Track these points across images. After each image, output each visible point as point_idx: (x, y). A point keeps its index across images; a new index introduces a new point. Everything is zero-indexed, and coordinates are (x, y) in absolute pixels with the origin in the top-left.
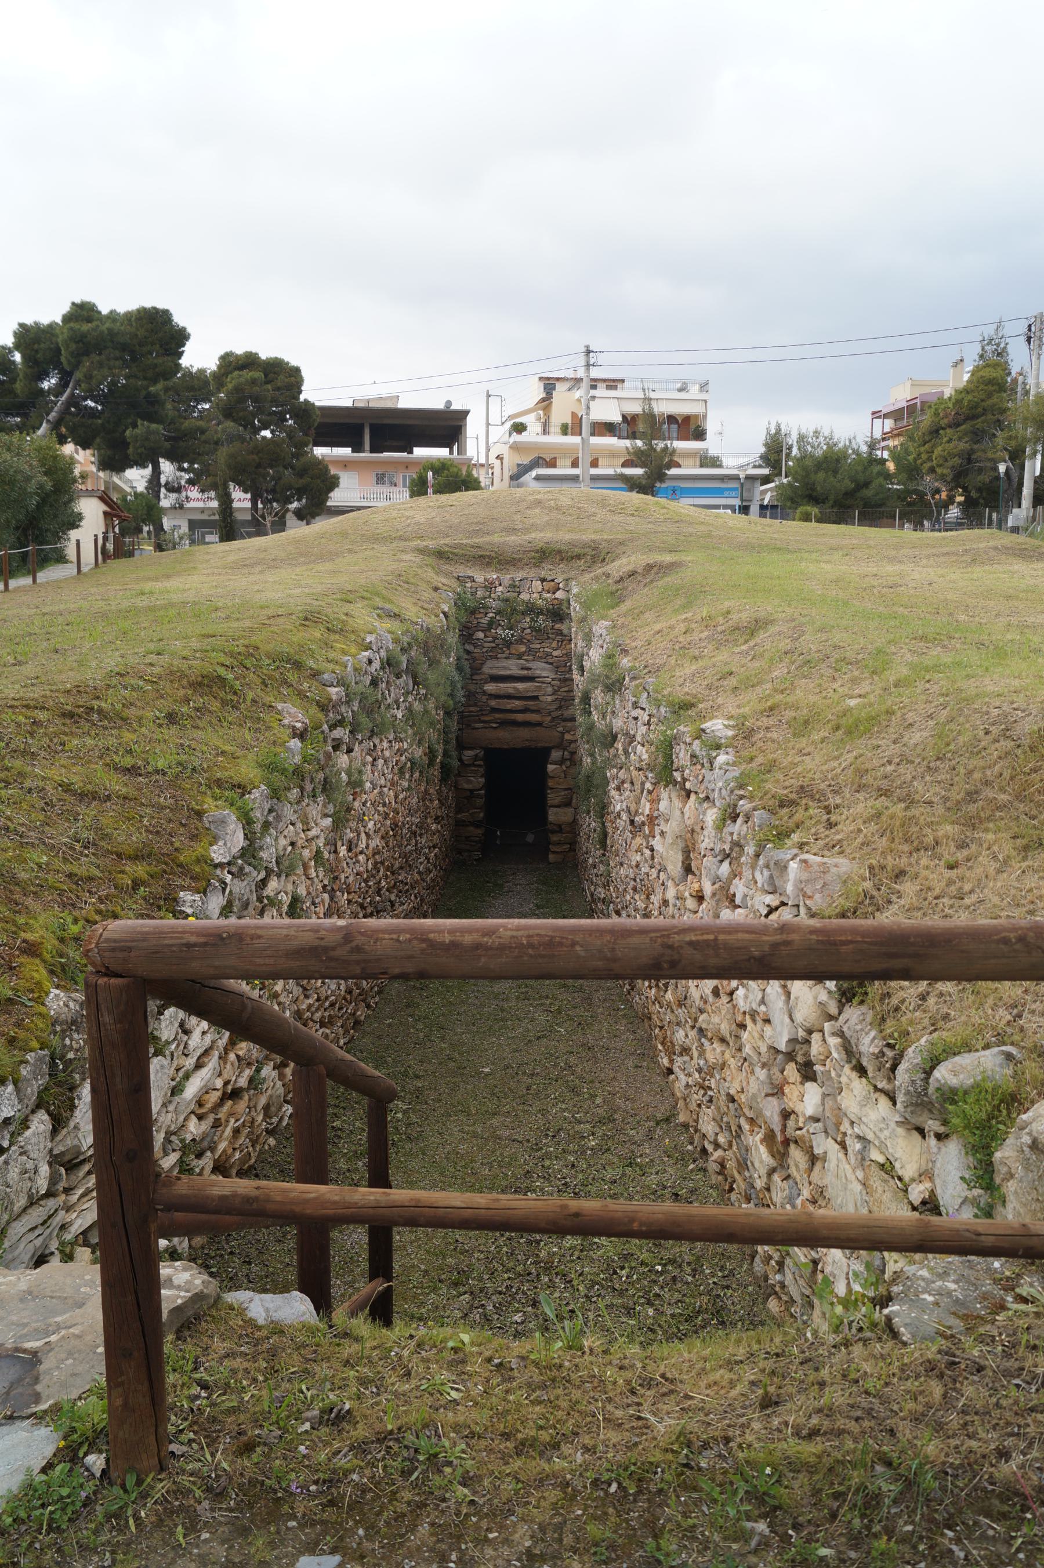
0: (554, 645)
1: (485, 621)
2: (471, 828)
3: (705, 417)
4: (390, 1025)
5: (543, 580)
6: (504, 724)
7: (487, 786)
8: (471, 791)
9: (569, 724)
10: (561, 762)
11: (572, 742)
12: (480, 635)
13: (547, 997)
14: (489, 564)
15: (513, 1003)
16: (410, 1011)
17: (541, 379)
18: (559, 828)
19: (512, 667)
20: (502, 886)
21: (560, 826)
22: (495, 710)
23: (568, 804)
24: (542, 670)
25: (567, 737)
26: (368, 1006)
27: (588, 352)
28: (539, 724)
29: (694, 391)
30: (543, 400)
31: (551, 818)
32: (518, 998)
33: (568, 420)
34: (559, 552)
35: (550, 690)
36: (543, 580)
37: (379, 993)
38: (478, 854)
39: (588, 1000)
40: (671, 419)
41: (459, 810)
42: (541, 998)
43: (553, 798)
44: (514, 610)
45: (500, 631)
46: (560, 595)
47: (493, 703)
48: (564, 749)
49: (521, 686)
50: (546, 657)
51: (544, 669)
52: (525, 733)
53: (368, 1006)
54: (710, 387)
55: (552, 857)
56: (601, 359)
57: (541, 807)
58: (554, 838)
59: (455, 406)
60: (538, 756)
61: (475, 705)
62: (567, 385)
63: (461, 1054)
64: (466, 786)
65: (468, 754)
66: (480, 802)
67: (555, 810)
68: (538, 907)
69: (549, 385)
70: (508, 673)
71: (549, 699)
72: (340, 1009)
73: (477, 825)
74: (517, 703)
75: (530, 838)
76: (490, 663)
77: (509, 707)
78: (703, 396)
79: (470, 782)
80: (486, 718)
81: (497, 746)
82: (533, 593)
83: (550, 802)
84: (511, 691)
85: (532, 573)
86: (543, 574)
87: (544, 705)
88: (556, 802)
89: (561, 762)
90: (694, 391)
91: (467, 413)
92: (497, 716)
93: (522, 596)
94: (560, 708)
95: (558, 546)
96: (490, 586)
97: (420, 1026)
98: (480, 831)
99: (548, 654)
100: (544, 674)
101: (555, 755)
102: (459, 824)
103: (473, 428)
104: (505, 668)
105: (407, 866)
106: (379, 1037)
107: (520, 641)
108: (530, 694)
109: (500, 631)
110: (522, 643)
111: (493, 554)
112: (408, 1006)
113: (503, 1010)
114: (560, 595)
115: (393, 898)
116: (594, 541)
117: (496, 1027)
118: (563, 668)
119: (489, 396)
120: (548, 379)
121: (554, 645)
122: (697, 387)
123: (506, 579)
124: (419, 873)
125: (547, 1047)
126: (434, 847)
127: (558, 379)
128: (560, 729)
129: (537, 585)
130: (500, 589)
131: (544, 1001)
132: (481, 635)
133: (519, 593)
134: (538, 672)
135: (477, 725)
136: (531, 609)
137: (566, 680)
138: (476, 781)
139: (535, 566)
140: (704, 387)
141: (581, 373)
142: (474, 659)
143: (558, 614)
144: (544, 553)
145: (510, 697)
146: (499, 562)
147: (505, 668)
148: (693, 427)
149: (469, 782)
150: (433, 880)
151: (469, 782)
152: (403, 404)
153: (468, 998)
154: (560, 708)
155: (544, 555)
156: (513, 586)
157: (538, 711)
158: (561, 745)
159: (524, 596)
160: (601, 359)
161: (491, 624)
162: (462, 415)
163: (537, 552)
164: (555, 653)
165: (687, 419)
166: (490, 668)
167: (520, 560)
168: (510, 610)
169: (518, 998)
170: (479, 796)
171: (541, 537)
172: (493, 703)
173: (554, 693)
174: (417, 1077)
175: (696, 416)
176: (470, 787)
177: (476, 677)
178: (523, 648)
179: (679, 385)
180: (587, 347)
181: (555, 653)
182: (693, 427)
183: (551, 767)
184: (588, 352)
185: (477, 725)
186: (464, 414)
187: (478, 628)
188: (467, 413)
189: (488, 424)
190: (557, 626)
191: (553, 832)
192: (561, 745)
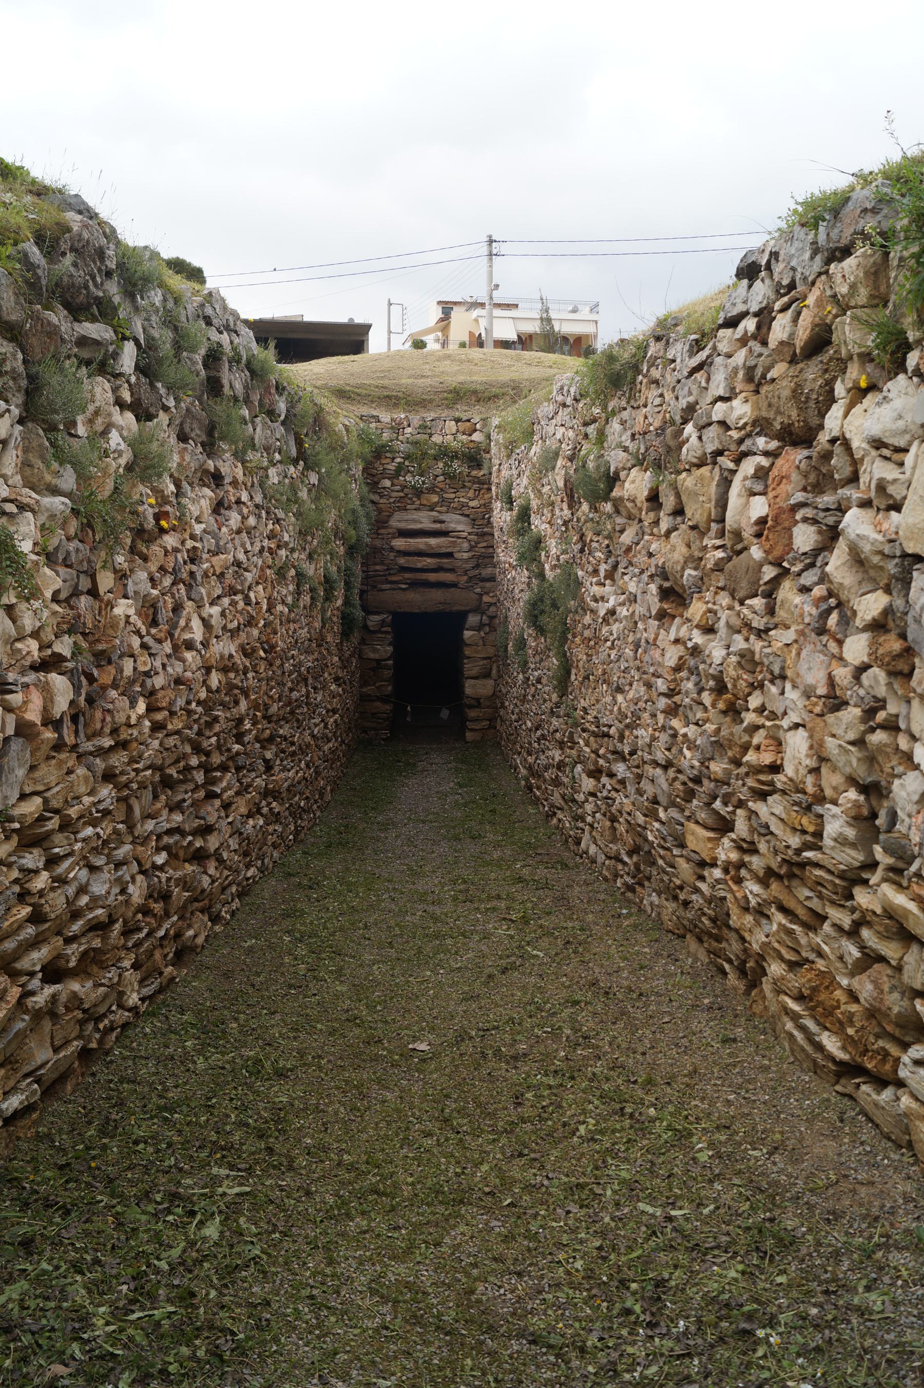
0: (471, 494)
1: (392, 467)
2: (378, 704)
3: (596, 336)
4: (250, 951)
5: (457, 420)
6: (415, 585)
7: (395, 656)
8: (378, 661)
9: (488, 585)
10: (479, 628)
11: (491, 604)
12: (387, 483)
13: (499, 897)
14: (396, 405)
15: (449, 907)
16: (287, 923)
17: (439, 303)
18: (477, 703)
19: (423, 520)
20: (414, 765)
21: (478, 700)
22: (404, 569)
23: (487, 675)
24: (457, 523)
25: (486, 599)
26: (216, 919)
27: (491, 241)
28: (454, 585)
29: (585, 313)
30: (442, 320)
31: (468, 691)
32: (455, 899)
33: (466, 339)
34: (475, 392)
35: (466, 545)
36: (457, 420)
37: (240, 895)
38: (385, 733)
39: (562, 900)
40: (565, 339)
41: (364, 683)
42: (490, 898)
43: (470, 668)
44: (424, 454)
45: (409, 478)
46: (476, 437)
47: (402, 561)
48: (483, 613)
49: (433, 541)
50: (461, 509)
51: (459, 522)
52: (437, 595)
53: (216, 919)
54: (600, 308)
55: (469, 736)
56: (503, 248)
57: (455, 678)
58: (472, 714)
59: (358, 320)
60: (454, 621)
61: (382, 563)
62: (463, 308)
63: (371, 1007)
64: (372, 656)
65: (374, 620)
66: (388, 673)
67: (472, 682)
68: (461, 786)
69: (447, 308)
70: (418, 526)
71: (466, 555)
72: (126, 933)
73: (384, 700)
74: (429, 560)
75: (445, 714)
76: (397, 516)
77: (419, 565)
78: (594, 317)
79: (377, 651)
80: (394, 578)
81: (407, 610)
82: (447, 434)
83: (467, 674)
84: (422, 547)
85: (446, 413)
86: (457, 414)
87: (459, 563)
88: (474, 672)
89: (479, 628)
90: (585, 313)
91: (368, 327)
92: (407, 575)
93: (434, 439)
94: (477, 566)
95: (473, 386)
96: (397, 428)
97: (301, 950)
98: (388, 707)
99: (464, 505)
100: (460, 528)
101: (473, 619)
102: (364, 699)
103: (376, 343)
104: (415, 521)
105: (291, 715)
106: (227, 975)
107: (432, 490)
108: (444, 550)
109: (409, 478)
110: (434, 492)
111: (400, 394)
112: (286, 915)
113: (436, 920)
114: (476, 437)
115: (269, 755)
116: (514, 381)
117: (428, 950)
118: (481, 522)
119: (390, 304)
120: (446, 303)
121: (471, 494)
122: (588, 309)
123: (416, 420)
124: (313, 736)
125: (524, 988)
126: (334, 711)
127: (455, 303)
128: (478, 590)
129: (451, 426)
130: (408, 430)
131: (495, 903)
132: (387, 483)
133: (431, 435)
134: (452, 526)
135: (384, 586)
136: (444, 453)
137: (484, 534)
138: (383, 650)
139: (448, 407)
140: (594, 308)
141: (483, 297)
142: (380, 511)
143: (474, 458)
144: (458, 393)
145: (420, 554)
146: (408, 403)
147: (415, 521)
148: (584, 346)
149: (375, 651)
150: (332, 752)
151: (375, 651)
152: (307, 319)
153: (380, 901)
154: (477, 566)
155: (457, 395)
156: (423, 427)
157: (452, 570)
158: (479, 609)
159: (437, 439)
160: (503, 248)
161: (399, 470)
162: (365, 329)
163: (450, 392)
164: (472, 504)
165: (579, 339)
166: (398, 521)
167: (431, 401)
168: (420, 455)
169: (455, 899)
170: (387, 667)
171: (452, 381)
172: (402, 561)
173: (471, 548)
174: (281, 1074)
175: (587, 336)
176: (377, 656)
177: (382, 531)
178: (435, 498)
179: (570, 308)
180: (490, 236)
181: (472, 504)
182: (584, 346)
183: (467, 634)
184: (491, 241)
185: (384, 586)
186: (366, 328)
187: (384, 475)
188: (368, 327)
189: (390, 332)
190: (474, 473)
191: (471, 707)
192: (479, 609)
